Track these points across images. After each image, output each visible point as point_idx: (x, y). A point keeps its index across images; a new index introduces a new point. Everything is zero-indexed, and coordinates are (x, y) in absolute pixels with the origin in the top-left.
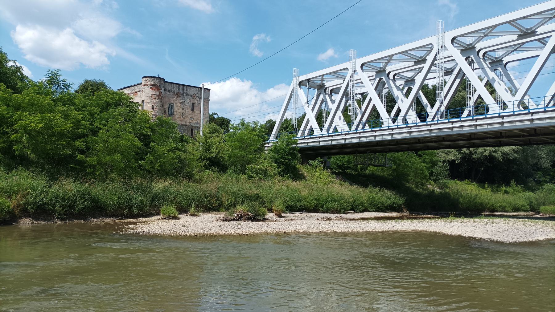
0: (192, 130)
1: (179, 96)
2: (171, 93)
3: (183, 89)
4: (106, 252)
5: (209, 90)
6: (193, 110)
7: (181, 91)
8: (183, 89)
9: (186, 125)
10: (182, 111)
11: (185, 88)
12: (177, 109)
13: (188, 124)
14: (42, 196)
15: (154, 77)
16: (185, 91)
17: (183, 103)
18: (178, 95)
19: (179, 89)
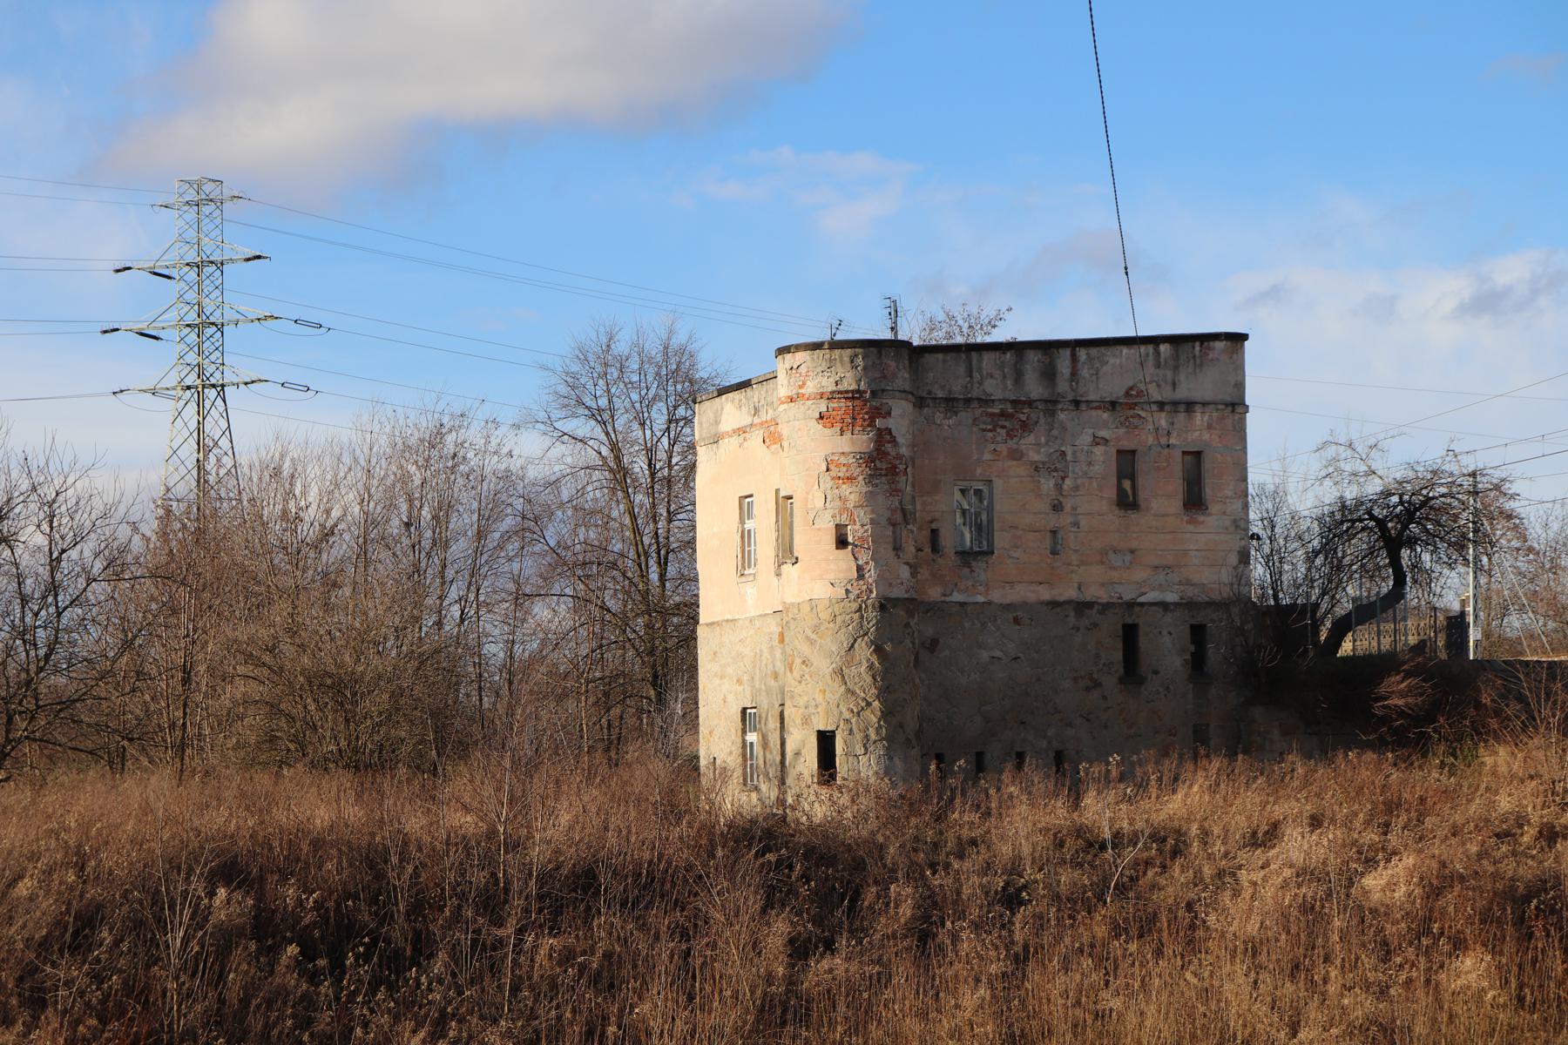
0: (1130, 634)
1: (1026, 427)
2: (965, 416)
3: (1049, 375)
4: (1190, 592)
5: (1238, 339)
6: (1127, 502)
7: (1034, 388)
8: (1049, 375)
9: (1082, 607)
10: (1053, 521)
11: (1063, 363)
12: (1017, 497)
13: (1094, 593)
14: (32, 653)
15: (817, 346)
16: (1063, 386)
17: (1056, 467)
18: (1013, 417)
19: (1019, 378)
